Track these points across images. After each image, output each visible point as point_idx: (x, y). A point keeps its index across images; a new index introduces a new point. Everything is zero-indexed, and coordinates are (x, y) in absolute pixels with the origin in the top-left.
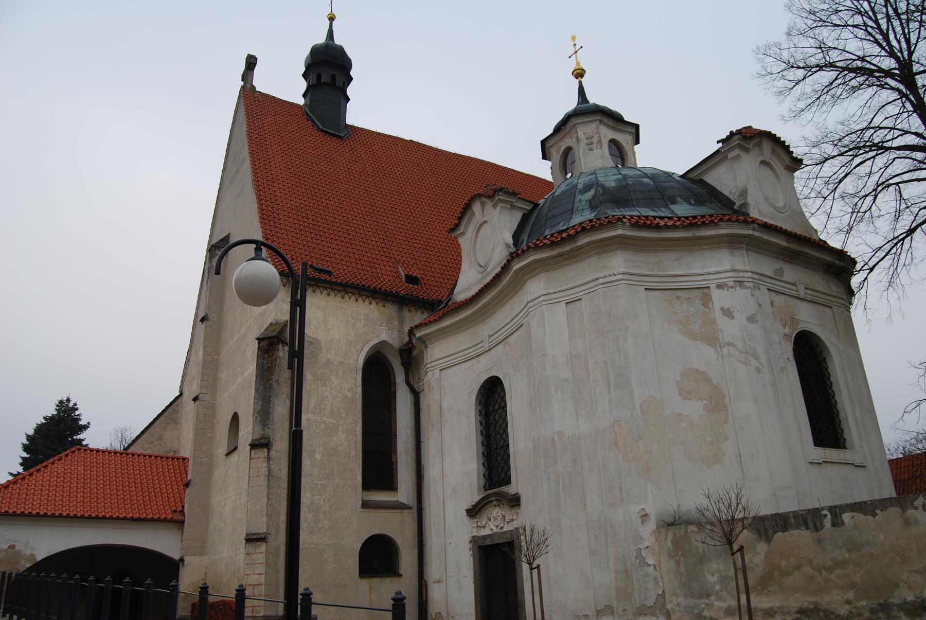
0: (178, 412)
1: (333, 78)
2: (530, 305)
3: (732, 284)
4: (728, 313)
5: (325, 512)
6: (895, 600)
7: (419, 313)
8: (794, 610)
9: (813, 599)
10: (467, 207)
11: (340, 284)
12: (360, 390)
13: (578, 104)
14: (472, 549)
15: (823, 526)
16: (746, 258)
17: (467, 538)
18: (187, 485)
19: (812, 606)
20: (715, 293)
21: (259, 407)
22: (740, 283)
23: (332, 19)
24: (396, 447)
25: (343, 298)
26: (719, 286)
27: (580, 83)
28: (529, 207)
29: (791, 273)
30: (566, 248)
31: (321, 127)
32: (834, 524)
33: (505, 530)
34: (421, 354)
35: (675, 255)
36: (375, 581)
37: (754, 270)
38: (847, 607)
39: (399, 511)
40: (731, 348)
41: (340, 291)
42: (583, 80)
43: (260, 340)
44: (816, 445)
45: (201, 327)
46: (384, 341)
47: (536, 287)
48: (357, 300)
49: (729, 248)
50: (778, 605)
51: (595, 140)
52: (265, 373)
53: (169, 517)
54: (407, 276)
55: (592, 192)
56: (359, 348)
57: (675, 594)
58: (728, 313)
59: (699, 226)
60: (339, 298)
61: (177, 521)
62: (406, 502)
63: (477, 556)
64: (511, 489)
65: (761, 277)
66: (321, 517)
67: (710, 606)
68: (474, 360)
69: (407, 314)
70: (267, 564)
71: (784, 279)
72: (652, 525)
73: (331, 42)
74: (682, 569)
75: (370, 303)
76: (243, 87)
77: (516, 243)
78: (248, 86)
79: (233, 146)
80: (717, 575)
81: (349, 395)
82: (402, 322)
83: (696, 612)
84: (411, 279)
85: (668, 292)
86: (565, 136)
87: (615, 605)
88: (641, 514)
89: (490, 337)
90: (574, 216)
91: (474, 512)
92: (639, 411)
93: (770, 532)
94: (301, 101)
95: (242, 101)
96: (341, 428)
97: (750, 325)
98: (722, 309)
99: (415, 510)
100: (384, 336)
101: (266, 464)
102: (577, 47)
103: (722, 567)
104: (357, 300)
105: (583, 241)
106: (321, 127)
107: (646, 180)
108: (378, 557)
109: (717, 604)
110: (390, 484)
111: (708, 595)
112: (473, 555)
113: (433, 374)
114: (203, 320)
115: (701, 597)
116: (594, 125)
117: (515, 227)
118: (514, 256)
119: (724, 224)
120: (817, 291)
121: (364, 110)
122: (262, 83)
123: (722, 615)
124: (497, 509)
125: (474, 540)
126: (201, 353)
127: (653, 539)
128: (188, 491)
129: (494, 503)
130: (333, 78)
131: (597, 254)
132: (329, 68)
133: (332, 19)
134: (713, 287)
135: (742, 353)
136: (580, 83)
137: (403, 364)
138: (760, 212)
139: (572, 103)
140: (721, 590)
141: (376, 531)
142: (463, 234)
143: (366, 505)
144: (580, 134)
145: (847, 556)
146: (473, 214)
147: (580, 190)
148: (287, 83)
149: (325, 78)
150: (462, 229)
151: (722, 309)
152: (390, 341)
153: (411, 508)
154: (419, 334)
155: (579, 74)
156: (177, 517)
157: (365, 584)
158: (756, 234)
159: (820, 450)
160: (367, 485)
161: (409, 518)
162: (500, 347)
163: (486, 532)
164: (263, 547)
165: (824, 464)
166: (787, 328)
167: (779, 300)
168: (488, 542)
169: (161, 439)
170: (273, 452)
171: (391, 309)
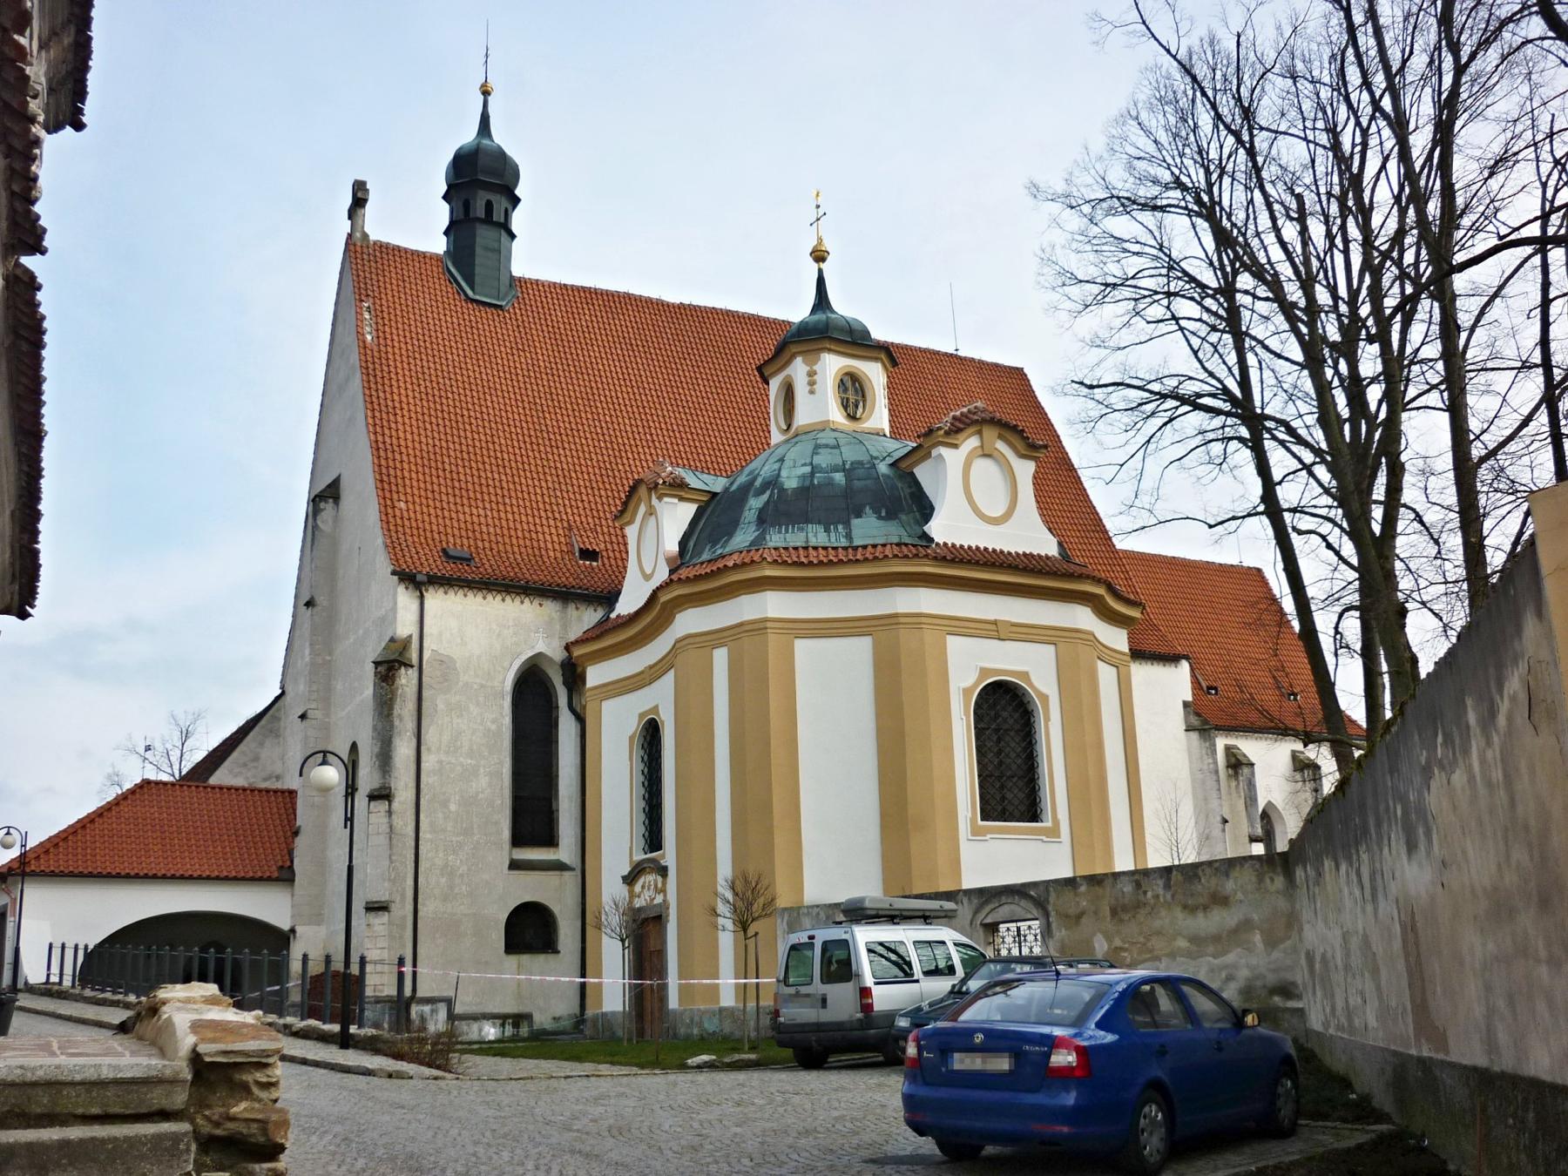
0: (279, 719)
1: (489, 205)
5: (462, 876)
12: (507, 720)
13: (813, 311)
18: (296, 833)
21: (376, 750)
23: (486, 93)
27: (820, 271)
31: (470, 293)
43: (377, 664)
45: (306, 613)
46: (540, 655)
52: (385, 705)
53: (276, 875)
56: (506, 664)
61: (285, 876)
66: (457, 881)
69: (571, 609)
70: (391, 937)
73: (486, 142)
76: (350, 236)
78: (358, 235)
79: (340, 329)
81: (493, 727)
82: (565, 627)
84: (589, 554)
91: (630, 880)
94: (439, 245)
95: (348, 276)
100: (541, 647)
101: (386, 820)
106: (470, 293)
107: (839, 477)
108: (529, 930)
110: (551, 841)
114: (309, 604)
117: (685, 527)
121: (540, 249)
122: (379, 227)
126: (307, 652)
128: (298, 840)
130: (489, 205)
132: (481, 186)
133: (486, 93)
136: (820, 271)
141: (528, 898)
148: (418, 222)
150: (627, 516)
152: (549, 653)
155: (819, 256)
156: (285, 875)
160: (518, 840)
161: (570, 880)
164: (384, 918)
169: (256, 759)
170: (395, 805)
171: (550, 608)
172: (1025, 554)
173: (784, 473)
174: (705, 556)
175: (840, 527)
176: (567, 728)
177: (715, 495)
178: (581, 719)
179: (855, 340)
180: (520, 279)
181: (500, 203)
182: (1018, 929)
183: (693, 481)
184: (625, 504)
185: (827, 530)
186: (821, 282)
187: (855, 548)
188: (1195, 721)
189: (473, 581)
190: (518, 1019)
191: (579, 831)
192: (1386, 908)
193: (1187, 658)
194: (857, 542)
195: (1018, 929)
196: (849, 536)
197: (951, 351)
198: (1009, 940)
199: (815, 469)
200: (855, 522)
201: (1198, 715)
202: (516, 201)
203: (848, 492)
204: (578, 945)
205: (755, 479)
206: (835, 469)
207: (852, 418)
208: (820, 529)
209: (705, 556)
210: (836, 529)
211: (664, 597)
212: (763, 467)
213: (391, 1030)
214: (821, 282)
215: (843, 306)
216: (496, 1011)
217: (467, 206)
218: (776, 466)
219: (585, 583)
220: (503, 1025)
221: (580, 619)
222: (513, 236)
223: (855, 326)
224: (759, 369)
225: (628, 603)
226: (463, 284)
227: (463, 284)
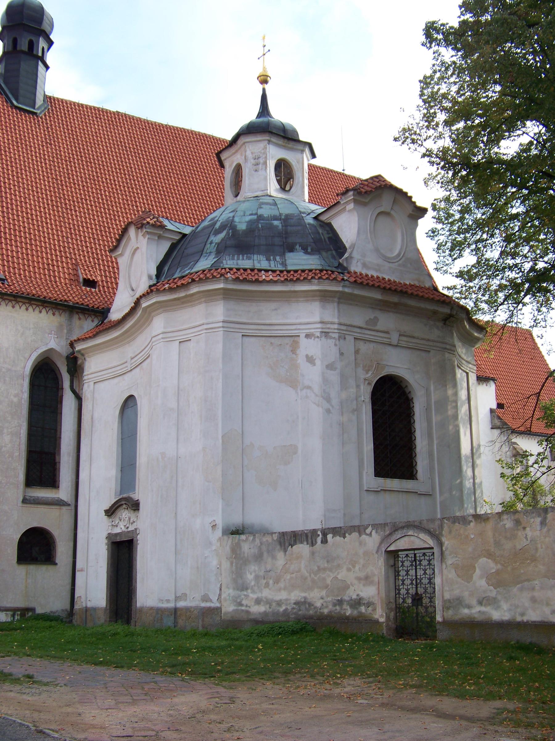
2: (154, 339)
3: (318, 334)
4: (310, 360)
6: (346, 598)
7: (89, 320)
8: (293, 602)
9: (303, 595)
10: (125, 230)
11: (11, 295)
12: (26, 396)
13: (259, 116)
14: (107, 544)
15: (316, 542)
16: (336, 311)
17: (105, 534)
19: (303, 600)
20: (303, 341)
22: (326, 334)
24: (60, 448)
25: (13, 307)
26: (308, 336)
27: (264, 90)
28: (177, 237)
29: (388, 321)
30: (182, 294)
31: (15, 103)
32: (322, 542)
33: (129, 529)
34: (83, 363)
35: (273, 305)
36: (32, 568)
37: (342, 321)
38: (321, 601)
39: (58, 507)
40: (309, 391)
41: (10, 301)
42: (266, 86)
44: (376, 476)
46: (51, 350)
47: (158, 324)
48: (27, 309)
49: (321, 301)
50: (284, 598)
51: (261, 161)
54: (84, 279)
55: (224, 233)
56: (27, 355)
57: (228, 587)
58: (310, 360)
59: (295, 281)
60: (9, 307)
62: (65, 500)
63: (110, 549)
64: (135, 497)
65: (349, 328)
67: (247, 596)
68: (121, 378)
71: (378, 327)
72: (219, 533)
74: (234, 568)
75: (40, 312)
77: (158, 276)
80: (253, 574)
81: (15, 400)
82: (70, 331)
83: (239, 601)
84: (90, 283)
85: (264, 339)
86: (237, 151)
87: (188, 593)
88: (212, 525)
89: (132, 359)
90: (202, 259)
91: (110, 512)
92: (221, 441)
93: (287, 544)
96: (5, 431)
97: (329, 371)
98: (307, 356)
99: (73, 507)
102: (266, 49)
103: (257, 568)
104: (27, 309)
105: (194, 289)
106: (15, 103)
108: (36, 547)
109: (251, 595)
110: (52, 482)
111: (247, 589)
112: (108, 549)
113: (89, 386)
115: (242, 590)
116: (262, 145)
117: (161, 257)
118: (151, 290)
119: (316, 281)
120: (414, 337)
123: (253, 604)
124: (126, 511)
125: (110, 536)
127: (219, 544)
129: (124, 506)
131: (206, 302)
134: (302, 336)
135: (317, 396)
136: (264, 90)
137: (69, 371)
138: (364, 265)
139: (250, 114)
140: (255, 585)
141: (35, 525)
142: (121, 255)
143: (25, 501)
144: (248, 153)
145: (326, 565)
146: (129, 239)
147: (216, 230)
149: (24, 46)
151: (307, 356)
152: (58, 348)
153: (69, 505)
154: (79, 347)
155: (264, 80)
157: (22, 570)
158: (347, 290)
159: (381, 480)
160: (30, 482)
161: (66, 513)
162: (137, 370)
163: (117, 530)
165: (382, 492)
166: (370, 373)
167: (364, 347)
168: (118, 539)
172: (411, 285)
173: (236, 219)
174: (177, 275)
175: (278, 258)
176: (68, 403)
177: (184, 235)
178: (79, 398)
179: (286, 136)
180: (50, 98)
181: (42, 43)
182: (415, 554)
183: (169, 226)
184: (119, 241)
185: (268, 260)
186: (264, 98)
187: (289, 272)
188: (497, 422)
189: (6, 294)
190: (25, 612)
191: (74, 477)
192: (470, 518)
193: (493, 379)
194: (289, 268)
195: (415, 554)
196: (284, 264)
197: (340, 170)
198: (407, 564)
199: (260, 217)
200: (289, 255)
201: (499, 418)
202: (51, 43)
203: (285, 234)
204: (71, 559)
205: (215, 223)
206: (275, 218)
207: (283, 189)
208: (262, 258)
209: (177, 275)
210: (275, 259)
211: (145, 304)
212: (221, 215)
213: (311, 201)
214: (264, 98)
215: (279, 114)
216: (8, 605)
217: (15, 42)
218: (231, 215)
219: (88, 309)
220: (13, 616)
221: (81, 327)
222: (47, 67)
223: (287, 127)
224: (218, 155)
225: (115, 315)
226: (10, 96)
227: (10, 96)
